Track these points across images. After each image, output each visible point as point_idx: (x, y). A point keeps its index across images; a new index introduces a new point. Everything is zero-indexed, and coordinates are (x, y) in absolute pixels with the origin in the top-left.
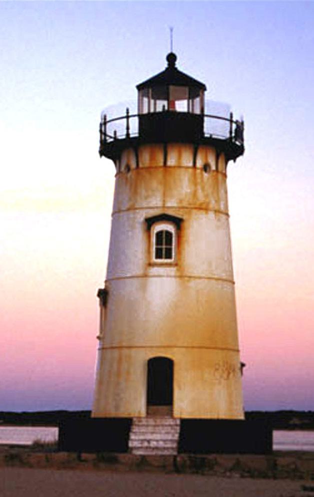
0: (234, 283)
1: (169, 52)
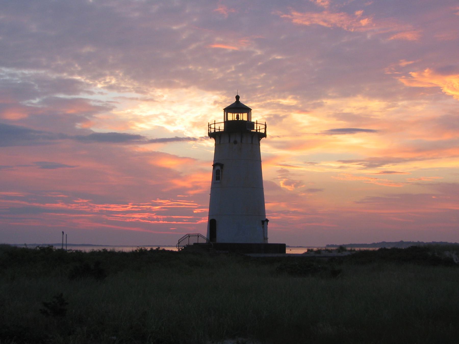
1: (237, 95)
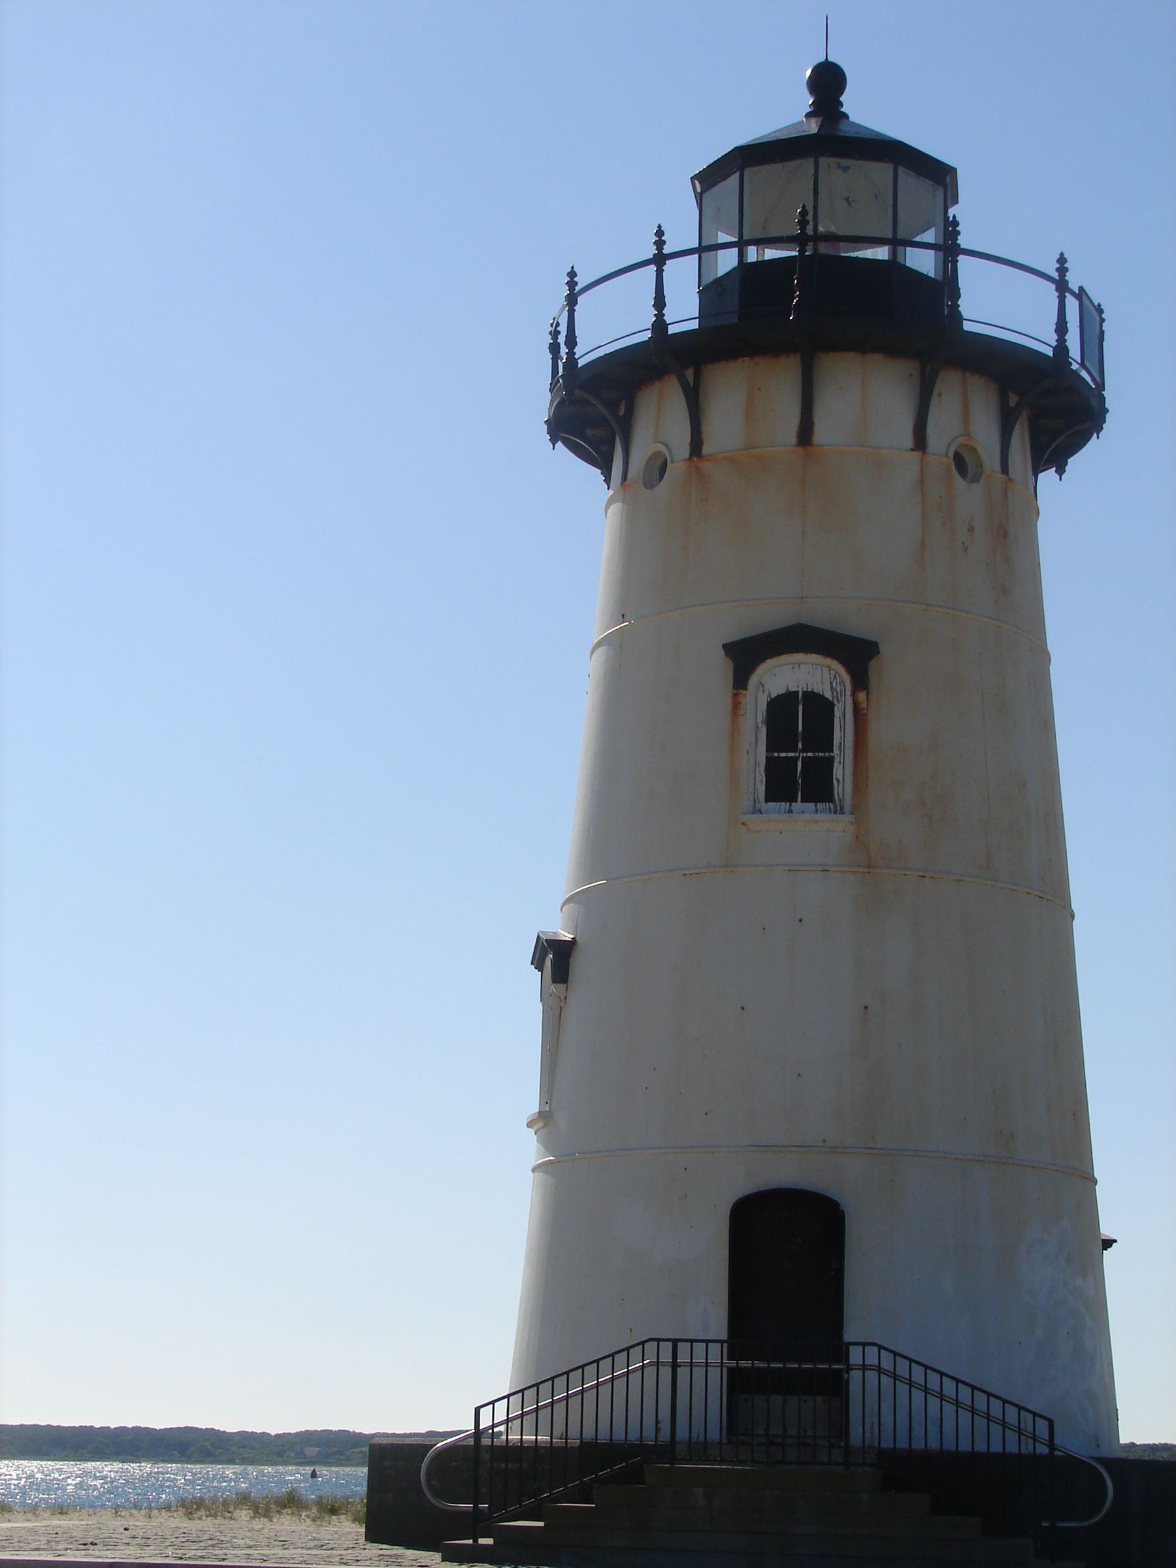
0: (975, 450)
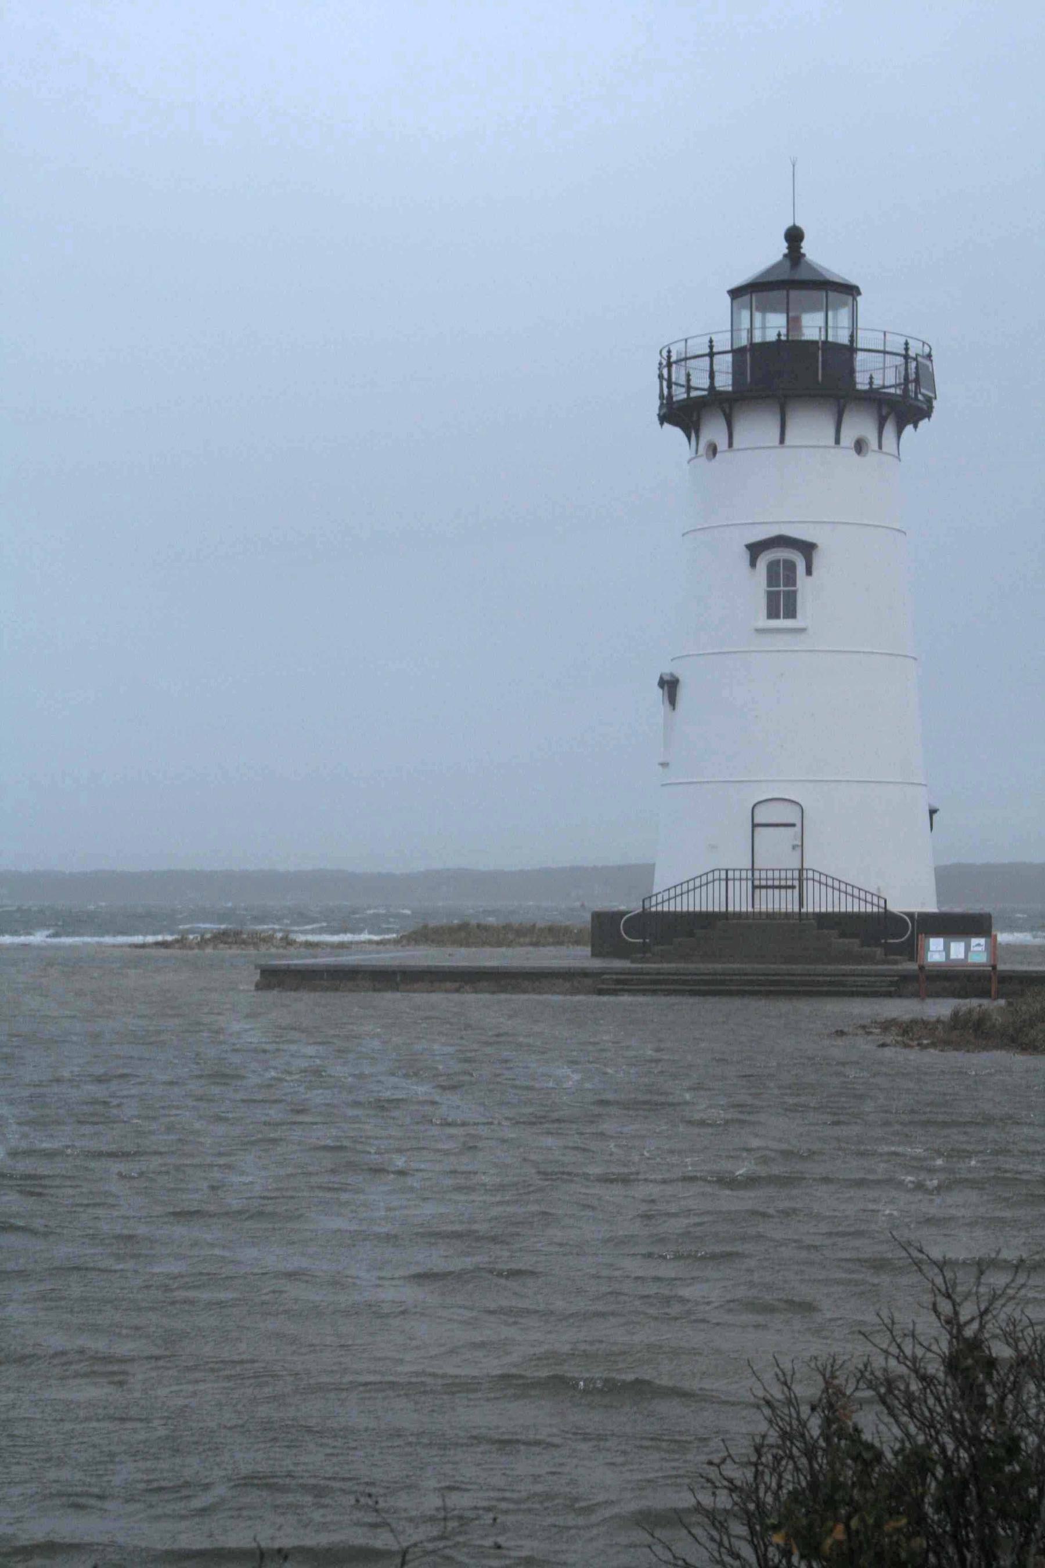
1: (790, 224)
